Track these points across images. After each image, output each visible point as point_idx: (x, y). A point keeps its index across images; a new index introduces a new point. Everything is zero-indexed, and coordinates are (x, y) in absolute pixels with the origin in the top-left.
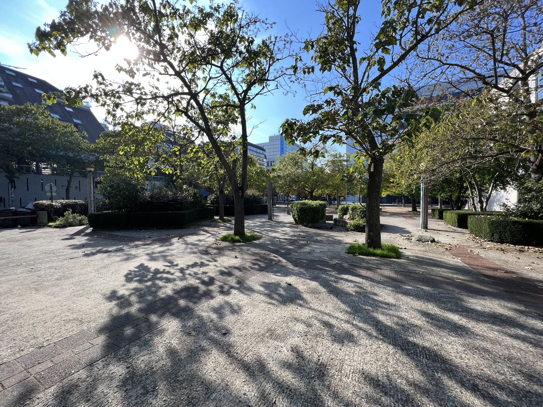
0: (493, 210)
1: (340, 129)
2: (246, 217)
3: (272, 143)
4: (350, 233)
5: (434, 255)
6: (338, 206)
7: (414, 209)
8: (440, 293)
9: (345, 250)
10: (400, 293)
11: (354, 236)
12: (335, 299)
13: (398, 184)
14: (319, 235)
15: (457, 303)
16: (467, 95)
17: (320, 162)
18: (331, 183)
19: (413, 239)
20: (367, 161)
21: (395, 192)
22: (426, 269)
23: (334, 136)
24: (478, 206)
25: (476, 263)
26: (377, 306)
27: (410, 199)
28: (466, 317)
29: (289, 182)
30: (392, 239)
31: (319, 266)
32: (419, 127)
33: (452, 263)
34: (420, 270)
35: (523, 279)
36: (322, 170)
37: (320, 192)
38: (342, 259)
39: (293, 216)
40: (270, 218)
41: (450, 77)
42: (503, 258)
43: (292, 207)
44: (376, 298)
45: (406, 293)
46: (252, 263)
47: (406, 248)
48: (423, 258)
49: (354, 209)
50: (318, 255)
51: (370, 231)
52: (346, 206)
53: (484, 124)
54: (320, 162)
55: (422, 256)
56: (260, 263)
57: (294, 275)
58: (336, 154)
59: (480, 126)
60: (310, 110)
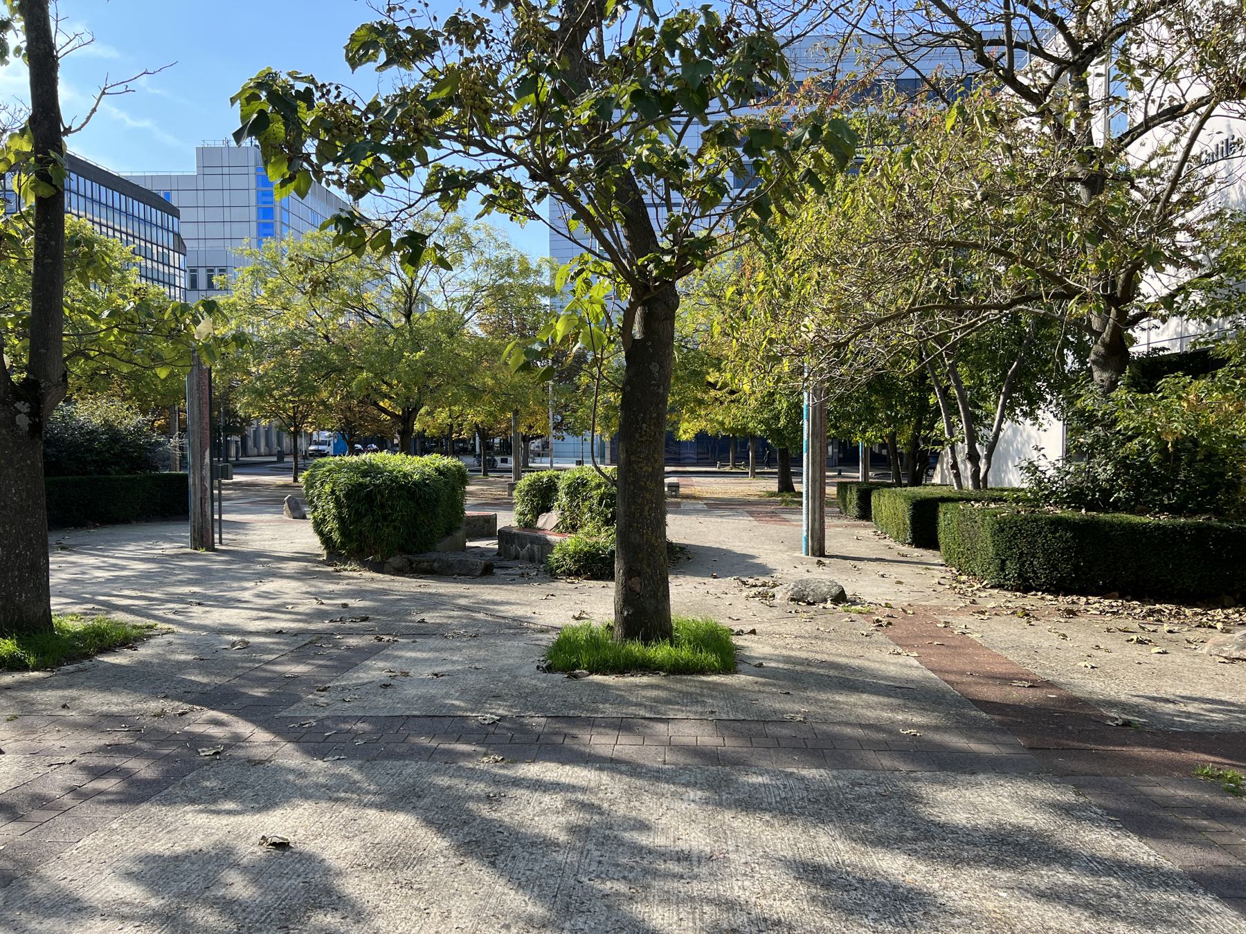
0: (1006, 486)
1: (509, 154)
2: (52, 538)
3: (216, 182)
4: (561, 584)
5: (842, 649)
6: (518, 478)
7: (786, 486)
8: (854, 784)
9: (537, 658)
10: (729, 807)
11: (576, 596)
12: (485, 875)
13: (732, 392)
14: (434, 602)
15: (902, 812)
16: (936, 92)
17: (440, 289)
18: (490, 382)
19: (778, 596)
20: (618, 297)
21: (722, 424)
22: (817, 701)
23: (486, 178)
24: (966, 469)
25: (959, 663)
26: (646, 872)
27: (769, 450)
28: (928, 856)
29: (302, 369)
30: (711, 600)
31: (423, 741)
32: (792, 183)
33: (892, 670)
34: (795, 708)
35: (1073, 701)
36: (451, 326)
37: (442, 416)
38: (527, 698)
39: (318, 526)
40: (203, 540)
41: (887, 18)
42: (1026, 640)
43: (311, 486)
44: (643, 839)
45: (750, 803)
46: (85, 768)
47: (753, 632)
48: (808, 662)
49: (578, 488)
50: (422, 691)
51: (629, 573)
52: (545, 475)
53: (979, 197)
54: (440, 289)
55: (804, 655)
56: (131, 764)
57: (307, 797)
58: (510, 260)
59: (967, 204)
60: (375, 45)
